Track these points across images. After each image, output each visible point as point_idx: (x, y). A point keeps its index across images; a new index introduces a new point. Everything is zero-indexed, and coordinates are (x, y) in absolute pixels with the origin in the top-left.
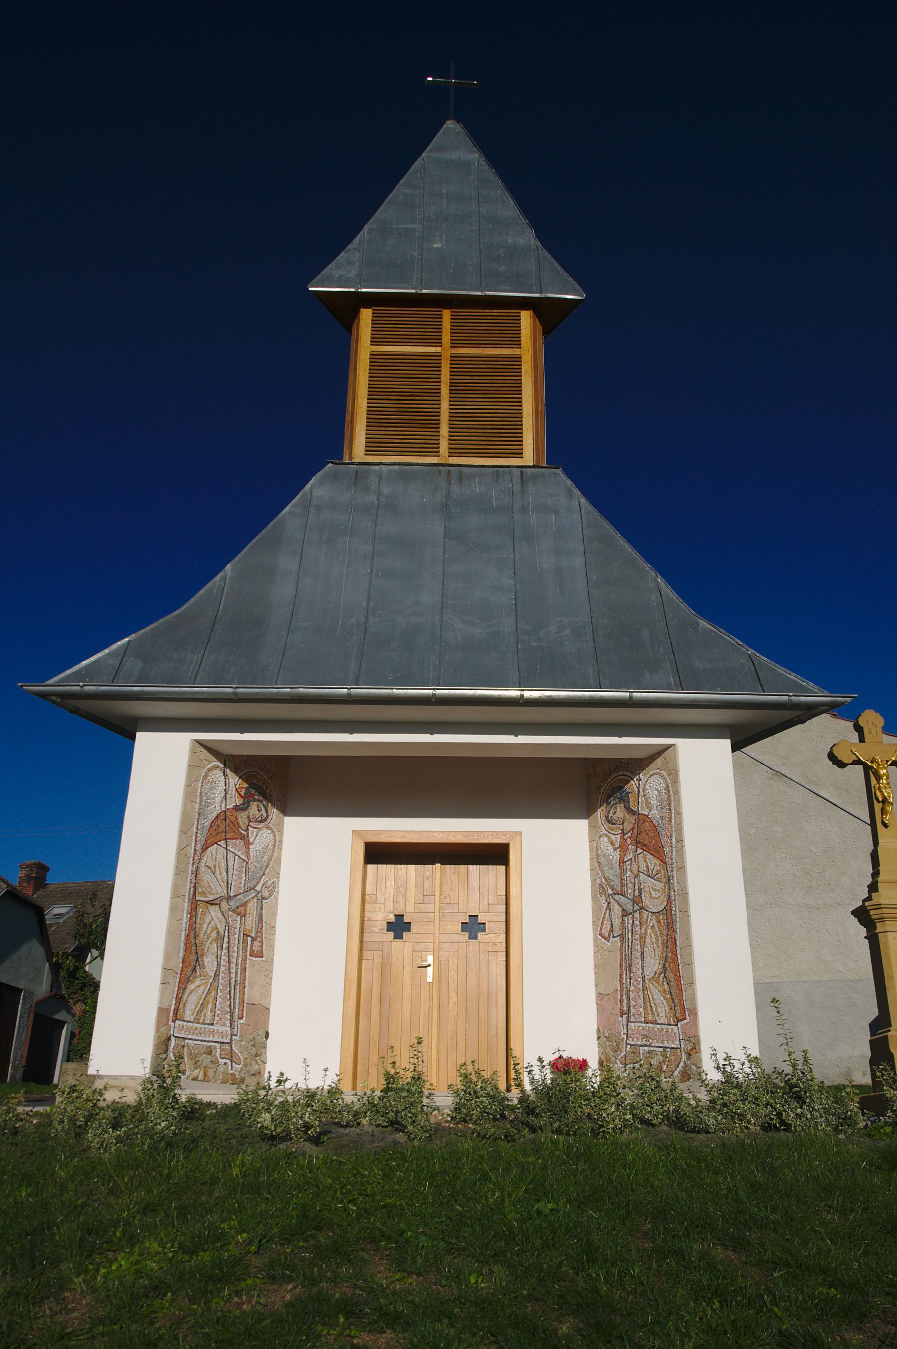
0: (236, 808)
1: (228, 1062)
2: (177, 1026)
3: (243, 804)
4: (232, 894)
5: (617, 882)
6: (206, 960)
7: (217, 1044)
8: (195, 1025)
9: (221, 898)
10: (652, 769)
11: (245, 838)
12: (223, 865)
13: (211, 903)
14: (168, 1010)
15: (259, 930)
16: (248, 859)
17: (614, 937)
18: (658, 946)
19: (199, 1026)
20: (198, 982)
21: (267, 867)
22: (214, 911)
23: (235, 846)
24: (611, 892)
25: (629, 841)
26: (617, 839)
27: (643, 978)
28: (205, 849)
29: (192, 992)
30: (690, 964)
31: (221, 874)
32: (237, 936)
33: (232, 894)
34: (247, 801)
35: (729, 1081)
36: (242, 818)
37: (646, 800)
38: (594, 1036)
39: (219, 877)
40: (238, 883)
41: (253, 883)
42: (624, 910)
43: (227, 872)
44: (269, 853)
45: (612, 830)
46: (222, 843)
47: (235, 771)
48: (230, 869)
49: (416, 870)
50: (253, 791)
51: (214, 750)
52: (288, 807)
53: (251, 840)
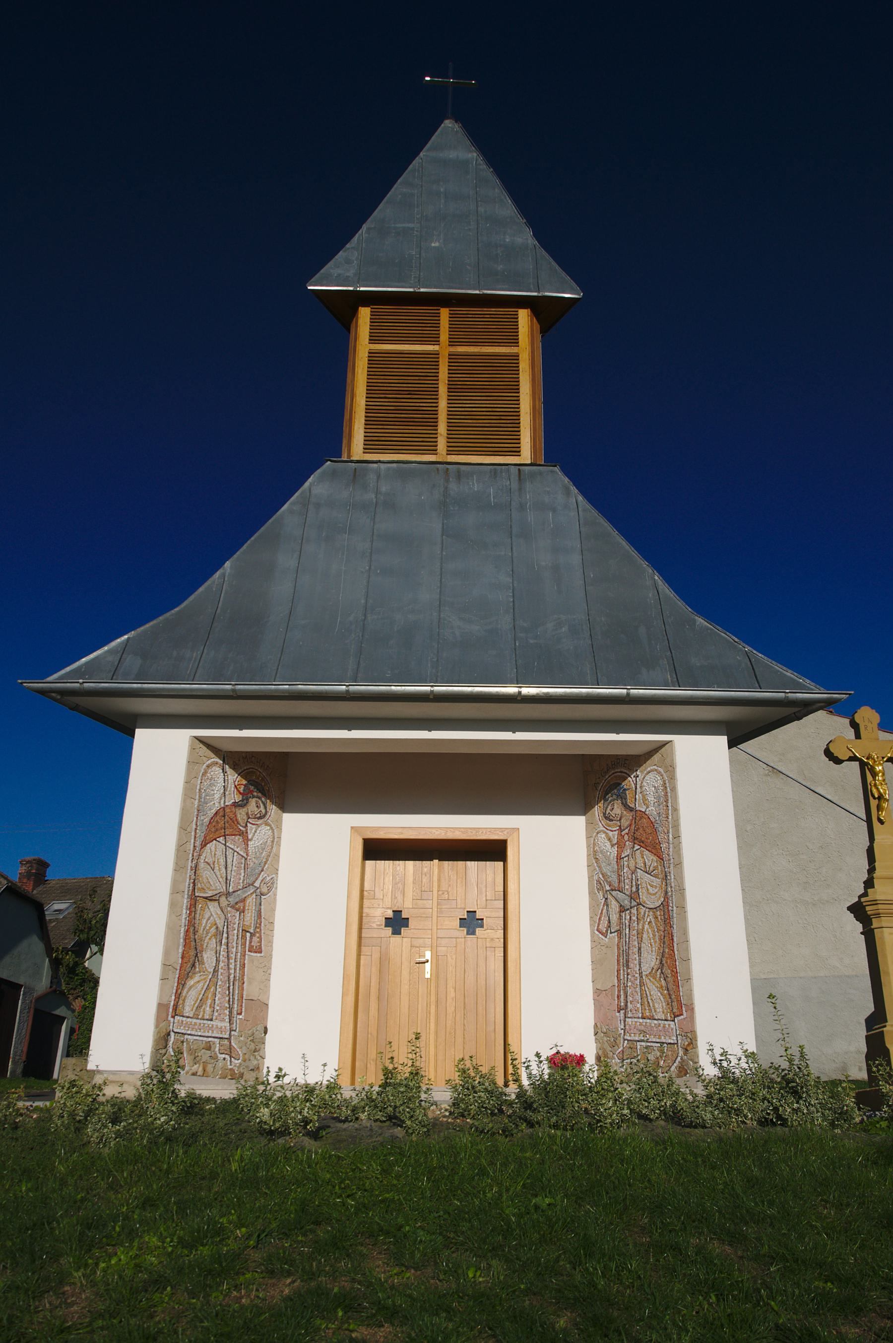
0: (235, 805)
1: (227, 1057)
2: (176, 1021)
3: (242, 800)
4: (231, 890)
5: (614, 878)
6: (205, 956)
7: (216, 1040)
8: (195, 1021)
9: (220, 894)
10: (649, 766)
11: (244, 835)
12: (222, 861)
13: (210, 899)
14: (168, 1006)
15: (258, 926)
16: (247, 855)
17: (611, 933)
18: (655, 942)
19: (198, 1021)
20: (197, 978)
21: (266, 863)
22: (213, 907)
23: (234, 843)
24: (608, 888)
25: (626, 837)
26: (614, 836)
27: (641, 974)
28: (204, 845)
29: (191, 988)
30: (687, 960)
31: (220, 870)
32: (236, 932)
33: (231, 890)
34: (246, 797)
35: (726, 1076)
36: (241, 814)
37: (644, 796)
38: (592, 1031)
39: (218, 873)
40: (237, 879)
41: (252, 879)
42: (621, 906)
43: (226, 868)
44: (268, 849)
45: (609, 826)
46: (221, 839)
47: (234, 767)
48: (229, 866)
49: (414, 866)
50: (252, 788)
51: (213, 747)
52: (287, 803)
53: (250, 837)
